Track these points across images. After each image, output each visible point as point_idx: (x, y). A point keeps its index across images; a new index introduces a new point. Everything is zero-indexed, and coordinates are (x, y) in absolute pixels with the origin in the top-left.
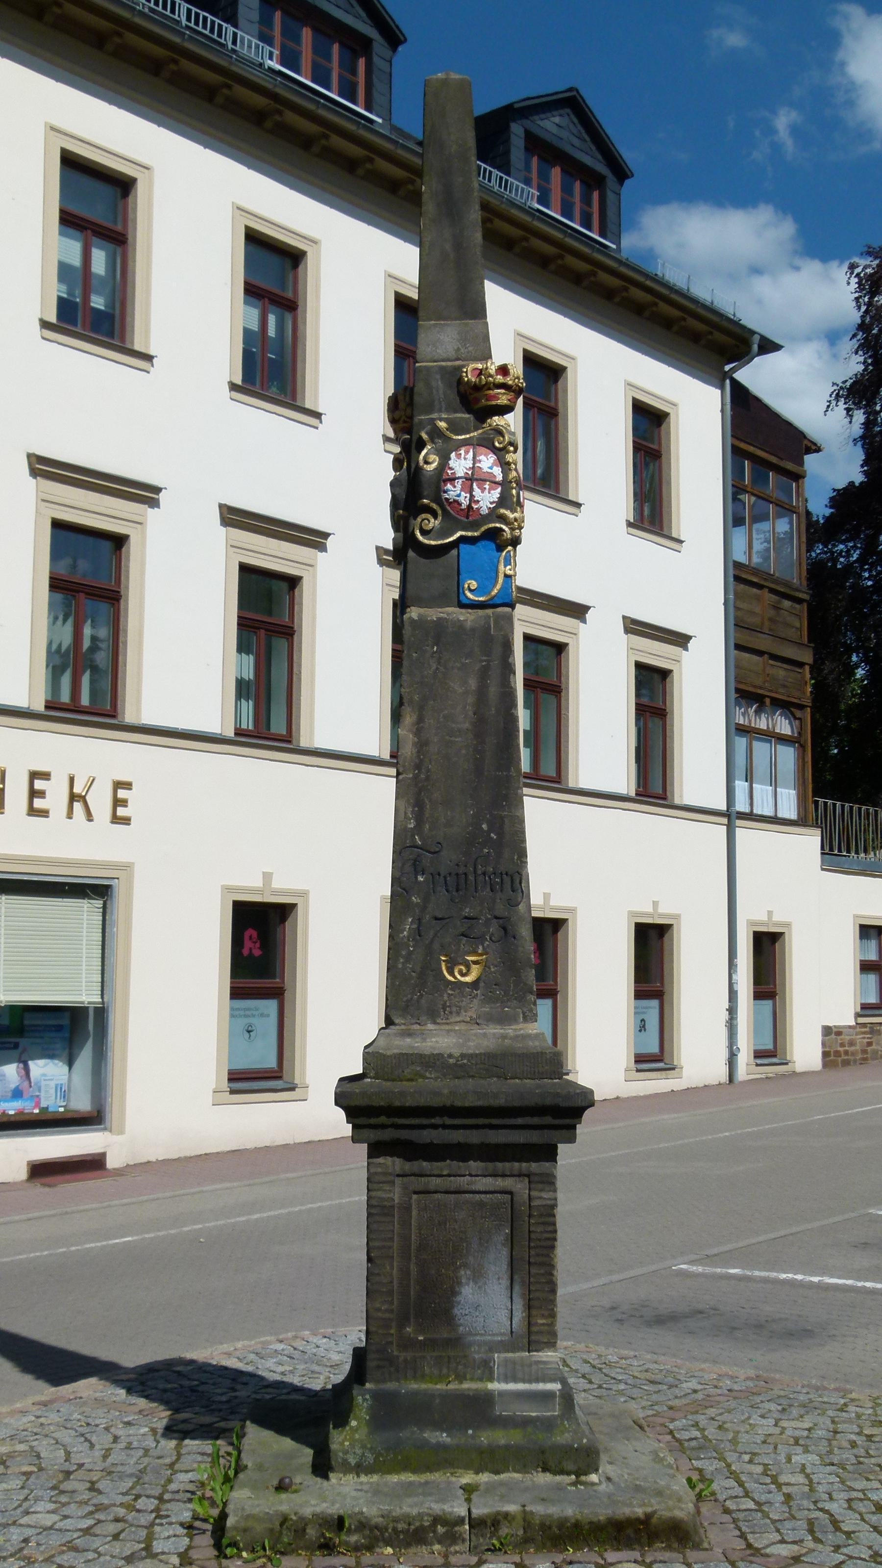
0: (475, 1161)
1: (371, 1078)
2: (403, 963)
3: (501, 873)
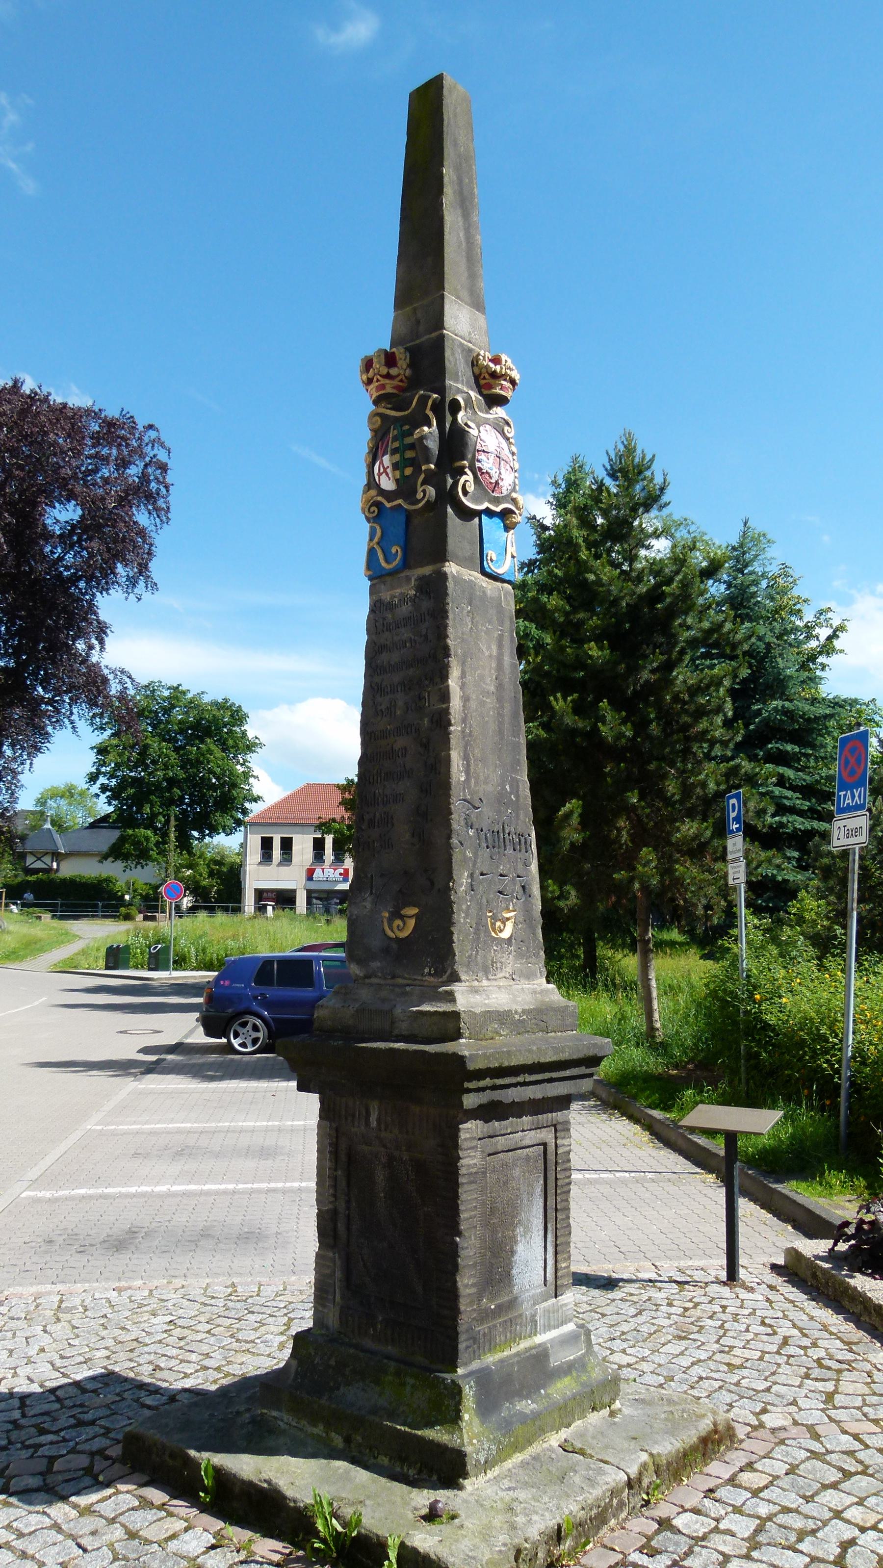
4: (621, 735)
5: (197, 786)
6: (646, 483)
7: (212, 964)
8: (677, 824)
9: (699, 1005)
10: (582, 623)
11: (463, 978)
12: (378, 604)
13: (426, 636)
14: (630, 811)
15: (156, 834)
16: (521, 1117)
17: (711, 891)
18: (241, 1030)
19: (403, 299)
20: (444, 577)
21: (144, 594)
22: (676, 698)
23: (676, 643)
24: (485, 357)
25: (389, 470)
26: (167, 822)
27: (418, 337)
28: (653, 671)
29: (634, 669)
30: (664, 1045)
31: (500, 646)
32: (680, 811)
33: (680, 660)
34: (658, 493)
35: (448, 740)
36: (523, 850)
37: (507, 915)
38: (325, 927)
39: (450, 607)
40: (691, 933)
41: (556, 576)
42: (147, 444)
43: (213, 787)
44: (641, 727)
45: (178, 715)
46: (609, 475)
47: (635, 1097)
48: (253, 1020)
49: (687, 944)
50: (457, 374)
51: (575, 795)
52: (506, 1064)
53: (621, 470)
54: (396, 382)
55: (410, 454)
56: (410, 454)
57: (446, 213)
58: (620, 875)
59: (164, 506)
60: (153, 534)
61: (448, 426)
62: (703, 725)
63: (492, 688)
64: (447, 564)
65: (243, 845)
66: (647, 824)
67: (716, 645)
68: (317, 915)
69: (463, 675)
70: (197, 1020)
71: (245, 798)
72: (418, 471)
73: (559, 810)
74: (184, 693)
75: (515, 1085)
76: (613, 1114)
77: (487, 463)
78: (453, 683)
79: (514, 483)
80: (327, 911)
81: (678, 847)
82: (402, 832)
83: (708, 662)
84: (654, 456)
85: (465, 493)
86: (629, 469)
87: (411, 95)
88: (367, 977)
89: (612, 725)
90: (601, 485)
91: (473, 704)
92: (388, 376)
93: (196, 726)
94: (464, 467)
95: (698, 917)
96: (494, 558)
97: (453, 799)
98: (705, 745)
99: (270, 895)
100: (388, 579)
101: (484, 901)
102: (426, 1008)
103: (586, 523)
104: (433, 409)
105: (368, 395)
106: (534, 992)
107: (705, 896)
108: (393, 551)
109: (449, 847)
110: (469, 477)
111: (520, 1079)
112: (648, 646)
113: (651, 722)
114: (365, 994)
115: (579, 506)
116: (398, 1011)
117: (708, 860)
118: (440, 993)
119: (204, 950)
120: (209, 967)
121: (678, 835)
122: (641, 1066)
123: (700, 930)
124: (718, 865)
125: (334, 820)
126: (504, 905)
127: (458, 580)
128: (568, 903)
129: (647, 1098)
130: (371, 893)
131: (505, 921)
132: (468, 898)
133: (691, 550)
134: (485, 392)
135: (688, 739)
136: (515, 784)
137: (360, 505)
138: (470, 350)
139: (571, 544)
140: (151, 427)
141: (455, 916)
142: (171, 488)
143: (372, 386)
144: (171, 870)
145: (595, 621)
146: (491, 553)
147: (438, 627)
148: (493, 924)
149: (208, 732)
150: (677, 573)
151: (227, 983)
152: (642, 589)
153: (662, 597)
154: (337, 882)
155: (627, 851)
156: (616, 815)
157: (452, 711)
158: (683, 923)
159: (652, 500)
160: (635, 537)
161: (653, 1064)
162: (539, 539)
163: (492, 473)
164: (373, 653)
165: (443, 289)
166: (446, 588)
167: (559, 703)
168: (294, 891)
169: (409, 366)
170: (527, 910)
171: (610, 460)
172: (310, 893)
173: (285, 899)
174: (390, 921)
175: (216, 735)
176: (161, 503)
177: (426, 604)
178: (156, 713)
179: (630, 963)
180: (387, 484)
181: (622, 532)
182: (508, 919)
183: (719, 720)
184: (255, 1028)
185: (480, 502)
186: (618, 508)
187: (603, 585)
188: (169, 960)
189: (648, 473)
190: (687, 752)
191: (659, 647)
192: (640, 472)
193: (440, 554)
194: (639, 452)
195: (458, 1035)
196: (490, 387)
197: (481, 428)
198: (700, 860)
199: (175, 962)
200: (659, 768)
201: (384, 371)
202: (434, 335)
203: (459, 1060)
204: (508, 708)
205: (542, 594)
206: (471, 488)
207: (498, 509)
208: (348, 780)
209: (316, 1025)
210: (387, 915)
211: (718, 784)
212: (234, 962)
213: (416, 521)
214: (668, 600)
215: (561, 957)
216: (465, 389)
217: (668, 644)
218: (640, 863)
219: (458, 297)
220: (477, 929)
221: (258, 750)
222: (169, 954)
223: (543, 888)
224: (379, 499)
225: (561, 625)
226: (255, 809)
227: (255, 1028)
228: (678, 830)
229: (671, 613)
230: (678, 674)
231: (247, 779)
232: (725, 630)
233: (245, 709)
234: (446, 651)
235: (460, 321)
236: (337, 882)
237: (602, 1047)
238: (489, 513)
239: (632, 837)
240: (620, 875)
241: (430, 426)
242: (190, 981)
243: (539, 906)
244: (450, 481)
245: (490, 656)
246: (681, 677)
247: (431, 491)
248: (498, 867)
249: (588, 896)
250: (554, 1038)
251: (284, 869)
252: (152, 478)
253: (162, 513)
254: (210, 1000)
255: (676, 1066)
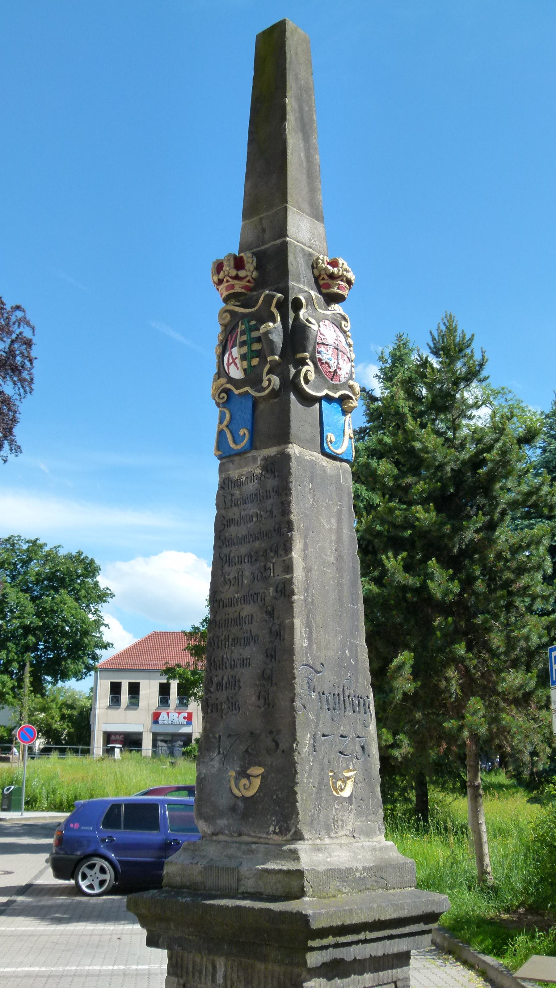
0: (368, 973)
1: (309, 896)
2: (307, 778)
3: (358, 697)
4: (448, 592)
5: (51, 632)
6: (466, 360)
7: (61, 804)
8: (503, 675)
9: (528, 848)
10: (408, 487)
11: (306, 836)
12: (227, 481)
13: (271, 511)
14: (458, 661)
15: (12, 679)
16: (361, 974)
17: (537, 738)
18: (88, 872)
19: (250, 210)
20: (286, 458)
21: (9, 456)
22: (499, 556)
23: (497, 505)
24: (324, 259)
25: (237, 361)
26: (22, 667)
27: (263, 243)
28: (477, 531)
29: (458, 530)
30: (495, 890)
31: (339, 520)
32: (505, 662)
33: (502, 520)
34: (478, 368)
35: (292, 609)
36: (362, 712)
37: (347, 774)
38: (170, 770)
39: (292, 485)
40: (518, 776)
41: (385, 444)
42: (14, 323)
43: (65, 634)
44: (467, 583)
45: (35, 567)
46: (432, 352)
47: (468, 942)
48: (100, 862)
49: (514, 786)
50: (299, 276)
51: (407, 647)
52: (348, 922)
53: (443, 349)
54: (244, 283)
55: (256, 347)
56: (256, 347)
57: (288, 137)
58: (450, 724)
59: (28, 377)
60: (17, 403)
61: (291, 321)
62: (525, 580)
63: (332, 559)
64: (290, 445)
65: (93, 690)
66: (475, 674)
67: (535, 505)
68: (162, 757)
69: (306, 547)
70: (47, 861)
71: (97, 646)
72: (264, 361)
73: (391, 661)
74: (41, 547)
75: (357, 943)
76: (447, 960)
77: (326, 355)
78: (296, 555)
79: (351, 371)
80: (172, 754)
81: (503, 696)
82: (249, 696)
83: (526, 523)
84: (473, 335)
85: (307, 381)
86: (450, 347)
87: (258, 37)
88: (214, 834)
89: (440, 582)
90: (425, 363)
91: (315, 574)
92: (237, 278)
93: (52, 577)
94: (304, 359)
95: (524, 764)
96: (333, 440)
97: (297, 665)
98: (526, 600)
99: (117, 737)
100: (236, 458)
101: (326, 761)
102: (271, 866)
103: (411, 395)
104: (278, 307)
105: (218, 294)
106: (374, 849)
107: (531, 743)
108: (241, 433)
109: (293, 709)
110: (310, 367)
111: (362, 936)
112: (471, 507)
113: (476, 578)
114: (212, 851)
115: (405, 380)
116: (244, 869)
117: (533, 709)
118: (285, 851)
119: (54, 792)
120: (59, 808)
121: (504, 685)
122: (473, 910)
123: (526, 774)
124: (543, 714)
125: (179, 666)
126: (344, 765)
127: (300, 460)
128: (402, 751)
129: (481, 943)
130: (219, 753)
131: (345, 780)
132: (311, 758)
133: (509, 419)
134: (324, 291)
135: (511, 594)
136: (354, 648)
137: (211, 391)
138: (311, 255)
139: (400, 417)
140: (18, 308)
141: (298, 776)
142: (35, 362)
143: (222, 286)
144: (25, 714)
145: (421, 486)
146: (330, 436)
147: (282, 503)
148: (334, 784)
149: (62, 583)
150: (497, 440)
151: (76, 826)
152: (465, 456)
153: (484, 462)
154: (181, 725)
155: (457, 699)
156: (445, 665)
157: (295, 581)
158: (510, 768)
159: (472, 375)
160: (457, 408)
161: (486, 908)
162: (369, 409)
163: (331, 363)
164: (222, 526)
165: (286, 202)
166: (289, 467)
167: (392, 562)
168: (140, 734)
169: (256, 268)
170: (366, 770)
171: (434, 339)
172: (155, 737)
173: (132, 742)
174: (237, 780)
175: (70, 585)
176: (25, 375)
177: (271, 483)
178: (15, 564)
179: (460, 806)
180: (236, 373)
181: (444, 403)
182: (348, 778)
183: (539, 576)
184: (103, 870)
185: (319, 389)
186: (441, 382)
187: (427, 452)
188: (21, 800)
189: (468, 351)
190: (509, 606)
191: (482, 509)
192: (461, 350)
193: (283, 436)
194: (459, 332)
195: (300, 893)
196: (328, 287)
197: (321, 324)
198: (525, 708)
199: (27, 803)
200: (486, 621)
201: (234, 273)
202: (278, 241)
203: (304, 919)
204: (347, 577)
205: (372, 459)
206: (312, 376)
207: (336, 395)
208: (194, 627)
209: (165, 881)
210: (234, 774)
211: (540, 637)
212: (84, 805)
213: (261, 406)
214: (490, 465)
215: (394, 802)
216: (307, 289)
217: (490, 506)
218: (469, 712)
219: (299, 209)
220: (319, 789)
221: (110, 600)
222: (21, 795)
223: (379, 736)
224: (229, 386)
225: (390, 489)
226: (105, 655)
227: (103, 870)
228: (504, 680)
229: (492, 478)
230: (501, 534)
231: (98, 627)
232: (543, 493)
233: (97, 562)
234: (289, 526)
235: (302, 231)
236: (181, 725)
237: (439, 904)
238: (328, 399)
239: (462, 687)
240: (450, 724)
241: (274, 322)
242: (41, 822)
243: (377, 765)
244: (293, 371)
245: (330, 530)
246: (503, 537)
247: (276, 380)
248: (339, 728)
249: (420, 745)
250: (394, 895)
251: (132, 713)
252: (17, 352)
253: (26, 385)
254: (60, 841)
255: (507, 910)
